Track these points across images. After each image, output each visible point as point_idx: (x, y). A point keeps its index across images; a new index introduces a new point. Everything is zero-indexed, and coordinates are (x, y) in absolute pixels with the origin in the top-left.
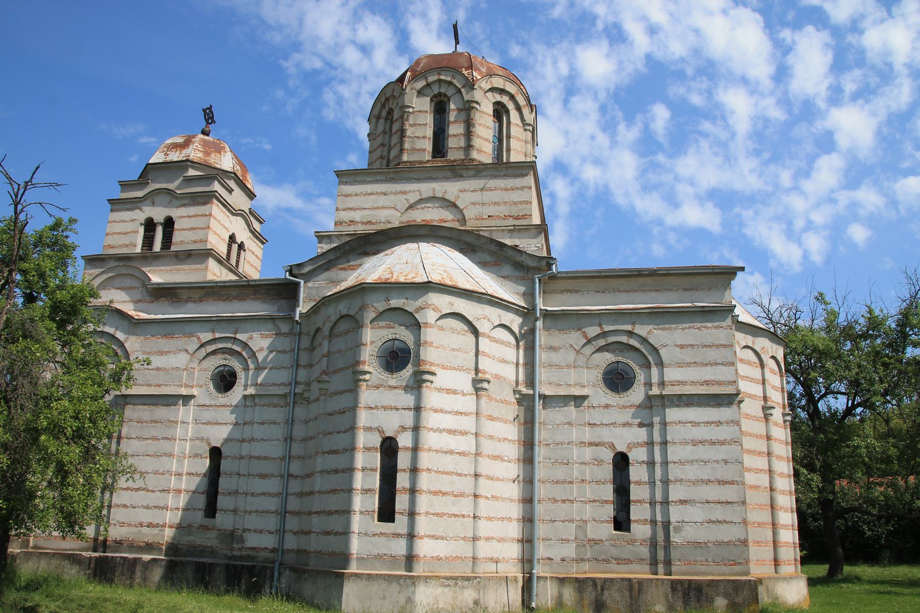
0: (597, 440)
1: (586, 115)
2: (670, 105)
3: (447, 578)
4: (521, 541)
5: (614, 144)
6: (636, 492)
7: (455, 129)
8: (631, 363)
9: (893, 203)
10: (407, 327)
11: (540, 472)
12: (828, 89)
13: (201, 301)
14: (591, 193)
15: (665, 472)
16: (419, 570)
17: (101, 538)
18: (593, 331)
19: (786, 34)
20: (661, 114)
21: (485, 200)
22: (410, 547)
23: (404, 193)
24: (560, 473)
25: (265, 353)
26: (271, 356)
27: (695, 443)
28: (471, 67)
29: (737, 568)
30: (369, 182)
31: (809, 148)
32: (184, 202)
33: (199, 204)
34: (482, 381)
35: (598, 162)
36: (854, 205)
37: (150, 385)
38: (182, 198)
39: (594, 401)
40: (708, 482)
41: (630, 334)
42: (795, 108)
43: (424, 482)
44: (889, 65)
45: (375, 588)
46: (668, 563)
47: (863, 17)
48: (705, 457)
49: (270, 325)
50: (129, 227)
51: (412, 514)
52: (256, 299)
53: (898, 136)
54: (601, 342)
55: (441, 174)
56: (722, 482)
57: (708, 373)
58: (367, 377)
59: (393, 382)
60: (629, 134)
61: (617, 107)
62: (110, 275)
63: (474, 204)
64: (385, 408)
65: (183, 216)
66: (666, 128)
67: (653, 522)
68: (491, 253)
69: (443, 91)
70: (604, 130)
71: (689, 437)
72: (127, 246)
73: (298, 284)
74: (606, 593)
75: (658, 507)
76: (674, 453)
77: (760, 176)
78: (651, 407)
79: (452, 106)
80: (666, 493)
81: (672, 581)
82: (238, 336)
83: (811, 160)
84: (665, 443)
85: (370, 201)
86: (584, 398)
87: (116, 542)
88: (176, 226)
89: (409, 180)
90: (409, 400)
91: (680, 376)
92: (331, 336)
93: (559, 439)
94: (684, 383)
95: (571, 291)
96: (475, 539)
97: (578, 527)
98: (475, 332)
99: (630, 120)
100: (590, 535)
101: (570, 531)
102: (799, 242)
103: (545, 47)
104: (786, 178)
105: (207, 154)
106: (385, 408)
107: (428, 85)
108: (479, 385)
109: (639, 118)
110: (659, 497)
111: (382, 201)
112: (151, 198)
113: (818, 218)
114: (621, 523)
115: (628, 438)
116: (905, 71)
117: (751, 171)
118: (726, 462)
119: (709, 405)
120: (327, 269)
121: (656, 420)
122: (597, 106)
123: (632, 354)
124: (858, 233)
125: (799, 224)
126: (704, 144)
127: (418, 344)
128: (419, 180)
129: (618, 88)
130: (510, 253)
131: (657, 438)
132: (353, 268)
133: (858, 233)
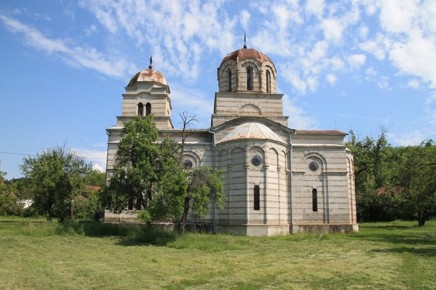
1: (210, 14)
2: (250, 11)
3: (275, 226)
4: (288, 215)
5: (223, 29)
6: (319, 200)
7: (256, 80)
8: (317, 162)
9: (347, 65)
10: (260, 152)
11: (293, 195)
12: (323, 10)
14: (211, 52)
15: (327, 195)
16: (268, 223)
18: (307, 152)
20: (246, 16)
21: (267, 106)
23: (240, 102)
24: (298, 195)
25: (202, 156)
26: (205, 158)
27: (336, 186)
28: (259, 57)
30: (228, 97)
31: (313, 38)
33: (160, 99)
35: (215, 37)
36: (331, 65)
40: (339, 197)
41: (317, 154)
42: (307, 18)
43: (268, 198)
46: (328, 220)
49: (203, 147)
50: (133, 106)
51: (265, 208)
53: (351, 36)
54: (309, 156)
55: (253, 96)
56: (343, 198)
57: (339, 166)
58: (249, 167)
59: (257, 169)
60: (230, 24)
61: (225, 11)
63: (264, 107)
64: (255, 177)
65: (155, 103)
66: (248, 23)
67: (324, 209)
68: (276, 127)
69: (250, 65)
70: (218, 22)
71: (334, 185)
72: (132, 113)
74: (312, 229)
75: (325, 204)
76: (330, 189)
78: (323, 176)
79: (254, 72)
80: (328, 200)
81: (330, 225)
82: (192, 150)
83: (313, 43)
84: (327, 186)
85: (228, 104)
86: (304, 173)
88: (152, 107)
90: (262, 174)
91: (331, 167)
92: (232, 153)
93: (297, 185)
96: (279, 214)
97: (303, 210)
98: (277, 153)
99: (231, 17)
100: (307, 213)
101: (301, 211)
102: (305, 80)
104: (301, 51)
106: (255, 177)
107: (245, 63)
109: (235, 17)
110: (325, 202)
111: (233, 104)
112: (141, 95)
113: (315, 70)
114: (315, 209)
115: (317, 184)
116: (357, 6)
117: (286, 46)
118: (344, 192)
119: (339, 175)
120: (223, 129)
121: (325, 179)
122: (215, 10)
123: (319, 160)
124: (331, 79)
125: (306, 72)
126: (265, 32)
127: (264, 157)
128: (245, 98)
130: (282, 127)
131: (325, 185)
133: (331, 79)
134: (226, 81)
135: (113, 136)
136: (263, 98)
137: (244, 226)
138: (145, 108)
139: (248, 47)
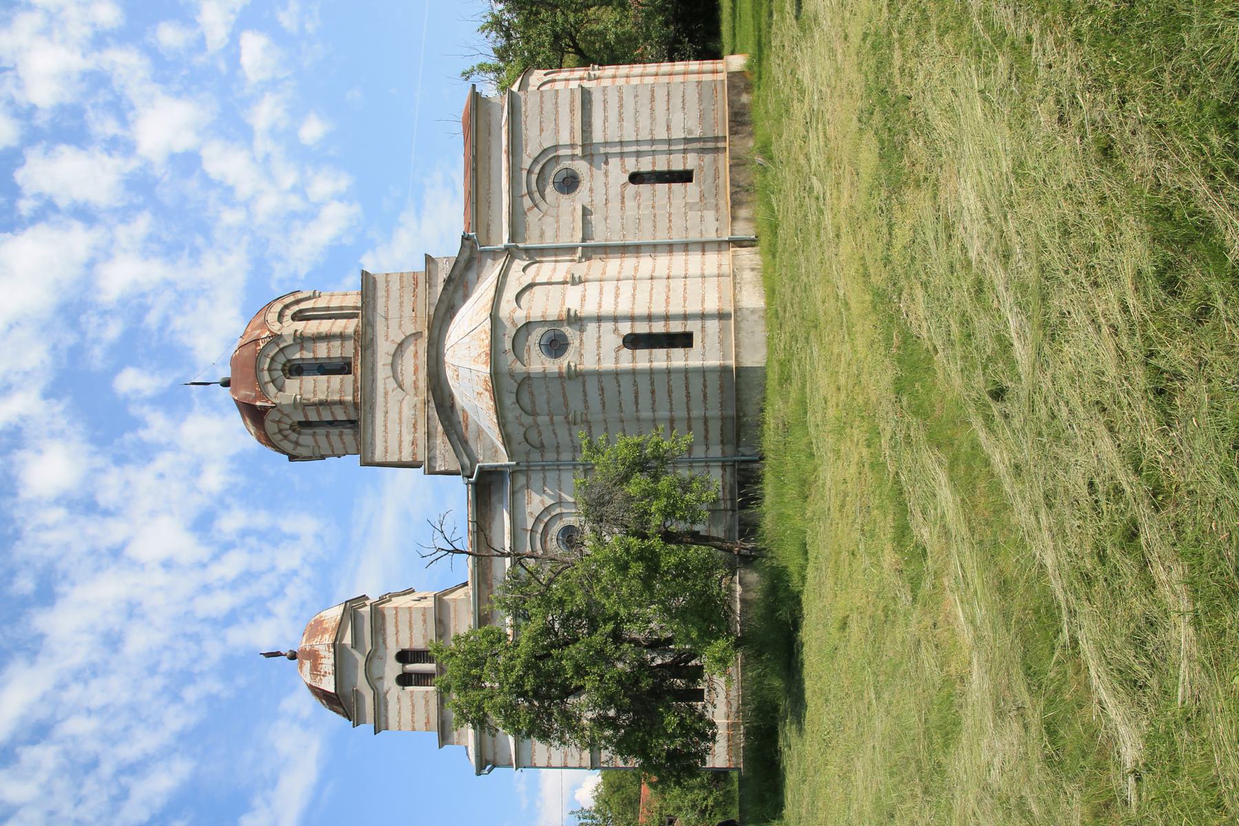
0: (619, 197)
2: (117, 369)
4: (703, 251)
5: (172, 447)
6: (661, 166)
7: (322, 350)
8: (554, 172)
9: (273, 85)
10: (529, 334)
11: (647, 239)
16: (729, 308)
18: (527, 202)
19: (25, 206)
20: (130, 381)
21: (397, 315)
22: (712, 316)
23: (386, 394)
24: (647, 225)
25: (546, 497)
27: (621, 120)
28: (256, 341)
29: (719, 88)
30: (373, 430)
32: (381, 641)
33: (383, 624)
34: (573, 277)
35: (197, 470)
36: (273, 133)
38: (377, 644)
39: (586, 202)
40: (652, 109)
41: (530, 172)
42: (135, 201)
43: (659, 309)
44: (85, 75)
45: (745, 340)
46: (716, 139)
47: (11, 102)
48: (632, 111)
49: (519, 495)
50: (406, 702)
52: (490, 527)
53: (185, 72)
54: (537, 195)
55: (369, 359)
58: (572, 364)
59: (577, 343)
60: (157, 425)
63: (400, 325)
64: (599, 347)
67: (685, 151)
68: (455, 291)
69: (280, 367)
71: (616, 124)
73: (480, 468)
74: (742, 184)
75: (673, 148)
76: (629, 135)
77: (227, 250)
78: (592, 155)
79: (298, 356)
82: (529, 528)
83: (208, 182)
84: (621, 143)
85: (393, 427)
86: (584, 208)
89: (373, 390)
90: (591, 327)
91: (566, 131)
92: (533, 413)
94: (572, 128)
95: (488, 231)
96: (703, 276)
97: (691, 209)
98: (531, 286)
101: (694, 215)
102: (319, 206)
103: (18, 543)
104: (231, 217)
105: (325, 630)
106: (599, 347)
107: (273, 381)
108: (576, 281)
109: (134, 411)
110: (665, 147)
111: (393, 415)
113: (289, 178)
114: (685, 177)
115: (617, 172)
118: (636, 96)
119: (590, 110)
120: (466, 442)
121: (602, 150)
123: (548, 168)
124: (313, 130)
125: (295, 202)
126: (178, 322)
127: (544, 322)
128: (374, 381)
129: (93, 440)
130: (457, 272)
131: (617, 149)
132: (466, 417)
133: (313, 130)
134: (327, 436)
135: (495, 753)
136: (373, 327)
138: (411, 667)
139: (226, 373)
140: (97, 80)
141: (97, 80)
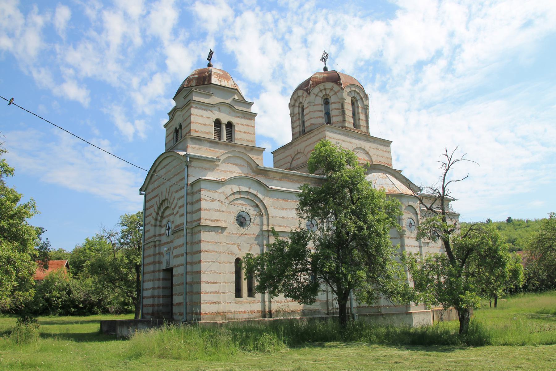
13: (280, 180)
17: (267, 310)
20: (63, 14)
23: (351, 143)
30: (337, 133)
32: (239, 115)
37: (280, 226)
38: (237, 112)
62: (230, 155)
83: (152, 74)
87: (276, 311)
102: (133, 123)
104: (135, 81)
128: (355, 138)
134: (321, 111)
135: (195, 167)
136: (373, 142)
137: (407, 314)
139: (329, 69)
140: (203, 35)
141: (203, 35)
